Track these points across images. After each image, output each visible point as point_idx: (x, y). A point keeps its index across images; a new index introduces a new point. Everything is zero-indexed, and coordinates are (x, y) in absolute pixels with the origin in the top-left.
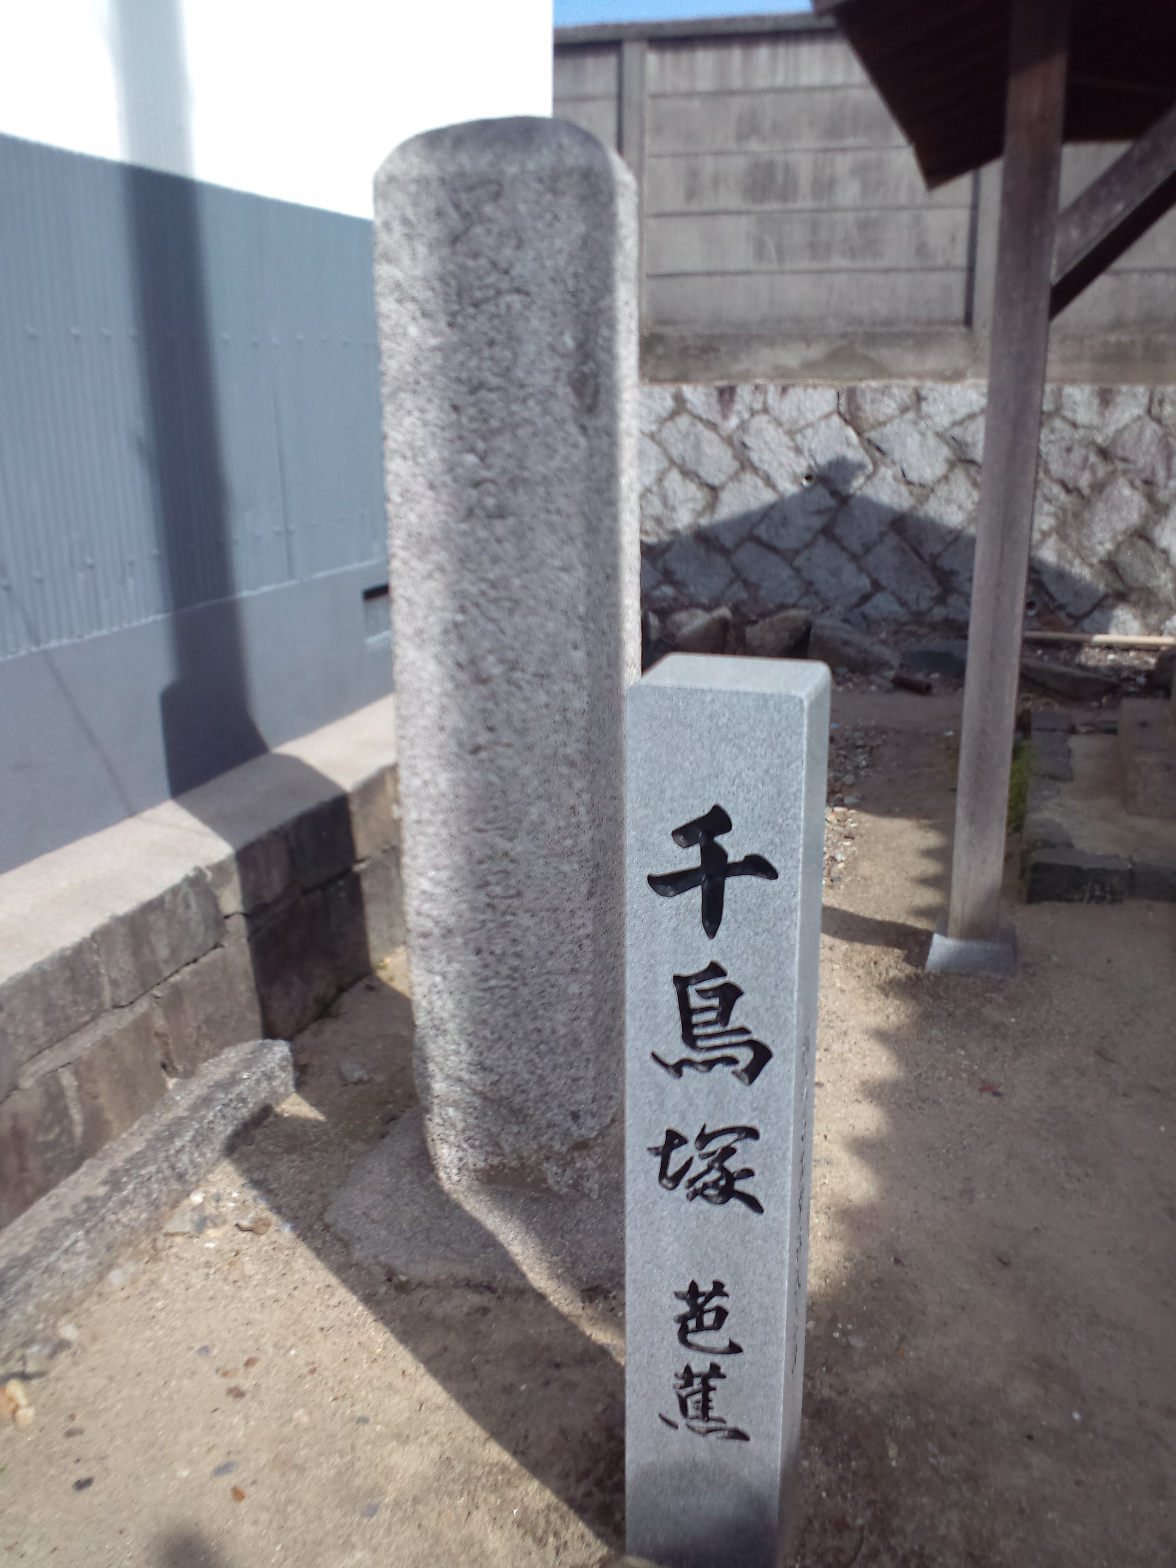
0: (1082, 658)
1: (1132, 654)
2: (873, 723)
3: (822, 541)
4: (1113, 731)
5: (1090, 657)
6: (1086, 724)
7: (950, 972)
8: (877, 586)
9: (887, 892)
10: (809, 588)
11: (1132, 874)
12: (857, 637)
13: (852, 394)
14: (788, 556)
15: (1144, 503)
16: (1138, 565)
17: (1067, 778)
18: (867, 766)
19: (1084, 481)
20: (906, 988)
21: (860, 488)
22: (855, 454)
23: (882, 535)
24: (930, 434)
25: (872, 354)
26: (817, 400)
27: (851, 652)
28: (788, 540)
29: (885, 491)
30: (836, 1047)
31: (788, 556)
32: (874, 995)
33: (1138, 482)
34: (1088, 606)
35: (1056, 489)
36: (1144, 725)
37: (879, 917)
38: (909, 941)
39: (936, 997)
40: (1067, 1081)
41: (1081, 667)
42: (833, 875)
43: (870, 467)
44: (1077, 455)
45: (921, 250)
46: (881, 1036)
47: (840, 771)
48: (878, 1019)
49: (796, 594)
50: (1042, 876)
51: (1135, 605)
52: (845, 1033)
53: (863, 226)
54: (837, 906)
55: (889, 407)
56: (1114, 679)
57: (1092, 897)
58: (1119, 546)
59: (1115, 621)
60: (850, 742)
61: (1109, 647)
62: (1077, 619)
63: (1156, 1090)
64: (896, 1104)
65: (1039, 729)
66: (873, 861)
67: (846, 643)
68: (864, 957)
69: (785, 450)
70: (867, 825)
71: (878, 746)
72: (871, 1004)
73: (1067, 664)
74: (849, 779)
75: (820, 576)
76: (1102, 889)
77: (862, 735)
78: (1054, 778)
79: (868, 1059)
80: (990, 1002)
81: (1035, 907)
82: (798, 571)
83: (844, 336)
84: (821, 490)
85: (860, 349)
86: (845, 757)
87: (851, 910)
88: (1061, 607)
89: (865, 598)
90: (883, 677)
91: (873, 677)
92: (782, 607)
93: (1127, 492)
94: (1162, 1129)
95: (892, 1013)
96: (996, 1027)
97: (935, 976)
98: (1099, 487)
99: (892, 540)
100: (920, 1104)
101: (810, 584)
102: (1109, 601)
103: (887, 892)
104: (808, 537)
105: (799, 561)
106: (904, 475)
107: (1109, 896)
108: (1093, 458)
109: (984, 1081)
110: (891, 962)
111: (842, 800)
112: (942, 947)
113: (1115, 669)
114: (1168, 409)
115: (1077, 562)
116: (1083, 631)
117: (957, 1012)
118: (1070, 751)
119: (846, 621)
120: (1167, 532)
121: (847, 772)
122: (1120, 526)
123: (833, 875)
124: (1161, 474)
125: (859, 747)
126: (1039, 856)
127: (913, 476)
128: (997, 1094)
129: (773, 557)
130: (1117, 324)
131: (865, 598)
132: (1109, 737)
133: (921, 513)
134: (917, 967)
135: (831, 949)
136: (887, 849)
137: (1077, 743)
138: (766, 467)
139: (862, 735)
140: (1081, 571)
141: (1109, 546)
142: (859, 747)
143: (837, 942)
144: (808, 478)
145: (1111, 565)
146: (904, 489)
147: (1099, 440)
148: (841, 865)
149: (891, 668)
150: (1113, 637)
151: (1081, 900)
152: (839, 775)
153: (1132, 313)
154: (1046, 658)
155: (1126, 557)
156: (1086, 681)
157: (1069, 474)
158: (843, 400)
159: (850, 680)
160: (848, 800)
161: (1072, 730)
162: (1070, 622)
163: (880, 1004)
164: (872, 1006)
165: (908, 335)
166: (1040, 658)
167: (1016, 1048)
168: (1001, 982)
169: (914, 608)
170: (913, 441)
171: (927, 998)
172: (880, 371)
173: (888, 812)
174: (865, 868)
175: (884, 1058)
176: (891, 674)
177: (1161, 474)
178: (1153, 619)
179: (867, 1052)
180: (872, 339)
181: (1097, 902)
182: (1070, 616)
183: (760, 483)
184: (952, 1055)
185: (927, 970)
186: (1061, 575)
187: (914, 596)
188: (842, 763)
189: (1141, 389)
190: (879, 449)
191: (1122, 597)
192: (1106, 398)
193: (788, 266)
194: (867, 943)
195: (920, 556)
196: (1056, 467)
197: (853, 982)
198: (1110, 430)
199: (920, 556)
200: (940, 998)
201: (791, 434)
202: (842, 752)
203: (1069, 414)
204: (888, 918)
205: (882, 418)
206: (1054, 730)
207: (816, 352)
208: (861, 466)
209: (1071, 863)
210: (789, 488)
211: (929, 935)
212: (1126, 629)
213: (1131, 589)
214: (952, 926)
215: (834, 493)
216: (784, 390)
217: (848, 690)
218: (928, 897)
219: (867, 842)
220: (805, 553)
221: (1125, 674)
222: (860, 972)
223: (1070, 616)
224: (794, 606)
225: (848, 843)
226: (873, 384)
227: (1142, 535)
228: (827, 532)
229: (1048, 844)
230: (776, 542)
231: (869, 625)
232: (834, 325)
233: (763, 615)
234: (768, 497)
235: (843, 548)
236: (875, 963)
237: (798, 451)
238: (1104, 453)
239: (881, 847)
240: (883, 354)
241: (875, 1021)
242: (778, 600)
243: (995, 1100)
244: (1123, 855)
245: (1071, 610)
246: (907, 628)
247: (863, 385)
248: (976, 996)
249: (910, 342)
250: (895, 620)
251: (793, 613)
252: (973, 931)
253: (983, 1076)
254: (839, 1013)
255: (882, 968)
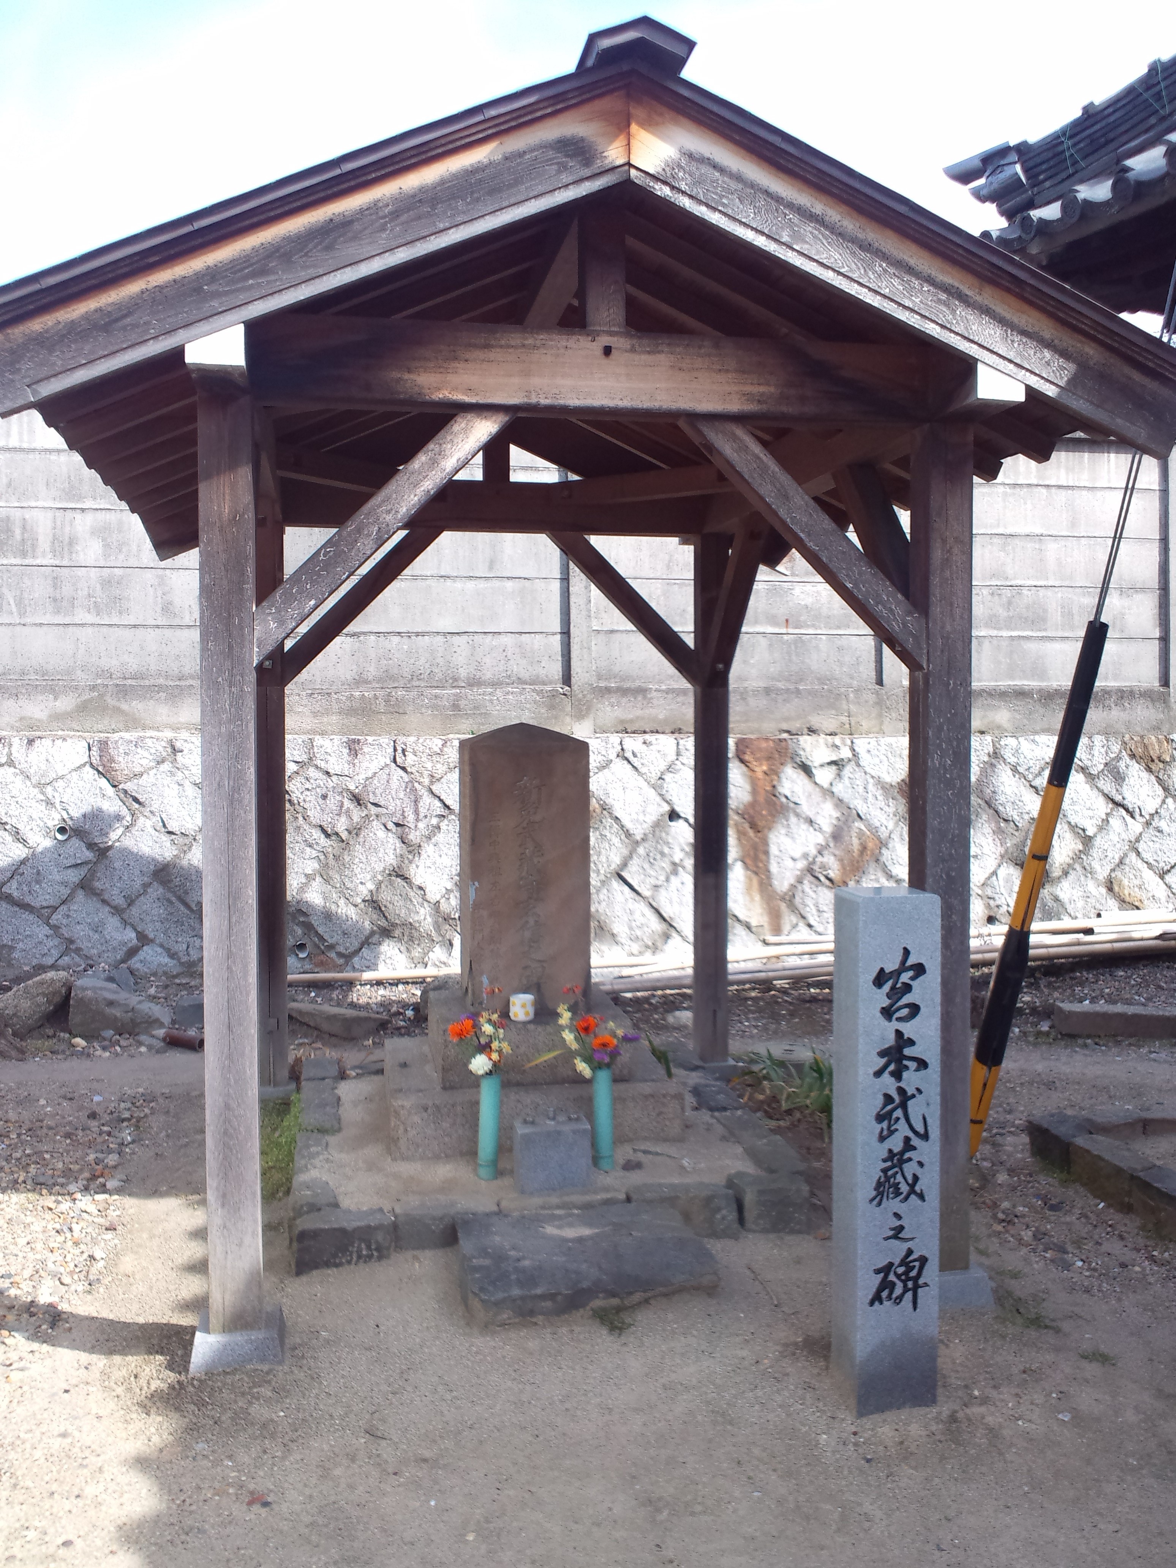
0: (354, 997)
1: (401, 987)
2: (141, 1090)
3: (80, 895)
4: (380, 1072)
5: (363, 995)
6: (354, 1068)
7: (221, 1370)
8: (143, 939)
9: (151, 1288)
10: (69, 945)
11: (395, 1226)
12: (122, 996)
13: (104, 745)
14: (44, 914)
15: (398, 844)
16: (399, 902)
17: (336, 1129)
18: (133, 1142)
19: (341, 826)
20: (170, 1399)
21: (118, 840)
22: (111, 804)
23: (146, 886)
24: (187, 783)
25: (124, 706)
26: (68, 753)
27: (117, 1012)
28: (43, 897)
29: (145, 842)
30: (90, 1490)
31: (44, 914)
32: (134, 1416)
33: (391, 826)
34: (356, 945)
35: (317, 834)
36: (404, 1065)
37: (141, 1320)
38: (170, 1342)
39: (201, 1404)
40: (337, 1472)
41: (353, 1005)
42: (91, 1277)
43: (129, 818)
44: (333, 801)
45: (167, 608)
46: (142, 1463)
47: (102, 1152)
48: (139, 1444)
49: (55, 953)
50: (309, 1244)
51: (400, 940)
52: (101, 1469)
53: (107, 583)
54: (95, 1315)
55: (142, 759)
56: (384, 1016)
57: (359, 1257)
58: (379, 885)
59: (382, 957)
60: (115, 1115)
61: (379, 983)
62: (348, 957)
63: (425, 1460)
64: (156, 1544)
65: (308, 1079)
66: (136, 1253)
67: (111, 1003)
68: (124, 1372)
69: (34, 803)
70: (132, 1211)
71: (146, 1116)
72: (131, 1427)
73: (339, 1005)
74: (112, 1159)
75: (80, 932)
76: (369, 1247)
77: (129, 1105)
78: (322, 1131)
79: (126, 1496)
80: (258, 1399)
81: (304, 1278)
82: (56, 928)
83: (93, 688)
84: (76, 842)
85: (111, 701)
86: (109, 1134)
87: (111, 1317)
88: (331, 947)
89: (132, 952)
90: (153, 1036)
91: (143, 1038)
92: (41, 969)
93: (381, 834)
94: (433, 1503)
95: (154, 1432)
96: (264, 1426)
97: (200, 1381)
98: (355, 831)
99: (156, 891)
100: (183, 1537)
101: (71, 941)
102: (375, 939)
103: (151, 1288)
104: (66, 892)
105: (56, 918)
106: (164, 826)
107: (375, 1254)
108: (347, 804)
109: (252, 1493)
110: (152, 1372)
111: (104, 1185)
112: (205, 1346)
113: (385, 1005)
114: (410, 759)
115: (342, 902)
116: (354, 969)
117: (223, 1418)
118: (339, 1099)
119: (110, 979)
120: (421, 870)
121: (110, 1151)
122: (379, 867)
123: (91, 1277)
124: (411, 818)
125: (123, 1120)
126: (306, 1223)
127: (173, 826)
128: (266, 1504)
129: (26, 915)
130: (360, 681)
131: (132, 952)
132: (376, 1078)
133: (185, 863)
134: (180, 1373)
135: (86, 1368)
136: (152, 1237)
137: (347, 1090)
138: (14, 821)
139: (129, 1105)
140: (346, 910)
141: (371, 886)
142: (123, 1120)
143: (94, 1358)
144: (62, 830)
145: (374, 904)
146: (165, 839)
147: (352, 787)
148: (101, 1264)
149: (162, 1025)
150: (383, 972)
151: (349, 1262)
152: (100, 1156)
153: (372, 671)
154: (319, 1000)
155: (385, 896)
156: (358, 1020)
157: (326, 820)
158: (95, 752)
159: (118, 1043)
160: (110, 1185)
161: (342, 1076)
162: (341, 961)
163: (141, 1425)
164: (133, 1428)
165: (160, 688)
166: (313, 1001)
167: (285, 1445)
168: (268, 1373)
169: (185, 959)
170: (171, 793)
171: (192, 1407)
172: (133, 722)
173: (155, 1193)
174: (128, 1263)
175: (144, 1491)
176: (161, 1032)
177: (411, 818)
178: (417, 952)
179: (126, 1488)
180: (123, 691)
181: (365, 1262)
182: (340, 955)
183: (9, 838)
184: (219, 1469)
185: (190, 1376)
186: (328, 916)
187: (185, 946)
188: (105, 1141)
189: (385, 740)
190: (136, 800)
191: (386, 933)
192: (354, 748)
193: (28, 620)
194: (126, 1355)
195: (187, 905)
196: (314, 814)
197: (112, 1405)
198: (361, 778)
199: (187, 905)
200: (205, 1404)
201: (41, 786)
202: (105, 1129)
203: (322, 765)
204: (151, 1320)
205: (138, 769)
206: (323, 1079)
207: (65, 703)
208: (118, 818)
209: (336, 1226)
210: (43, 842)
211: (192, 1331)
212: (393, 962)
213: (394, 925)
214: (213, 1320)
215: (91, 846)
216: (31, 742)
217: (117, 1055)
218: (192, 1287)
219: (130, 1232)
220: (64, 908)
221: (394, 1009)
222: (120, 1390)
223: (340, 955)
224: (54, 967)
225: (109, 1235)
226: (127, 735)
227: (399, 874)
228: (85, 885)
229: (314, 1208)
230: (28, 899)
231: (137, 980)
232: (83, 678)
233: (18, 980)
234: (19, 852)
235: (104, 902)
236: (136, 1377)
237: (49, 803)
238: (357, 799)
239: (145, 1236)
240: (136, 706)
241: (135, 1446)
242: (35, 962)
243: (264, 1512)
244: (387, 1207)
245: (341, 949)
246: (177, 981)
247: (116, 736)
248: (243, 1394)
249: (163, 695)
250: (165, 973)
251: (51, 974)
252: (238, 1321)
253: (252, 1486)
254: (93, 1447)
255: (143, 1382)
